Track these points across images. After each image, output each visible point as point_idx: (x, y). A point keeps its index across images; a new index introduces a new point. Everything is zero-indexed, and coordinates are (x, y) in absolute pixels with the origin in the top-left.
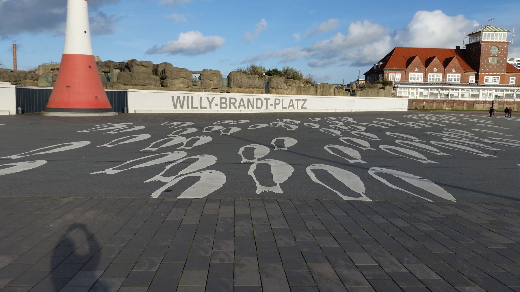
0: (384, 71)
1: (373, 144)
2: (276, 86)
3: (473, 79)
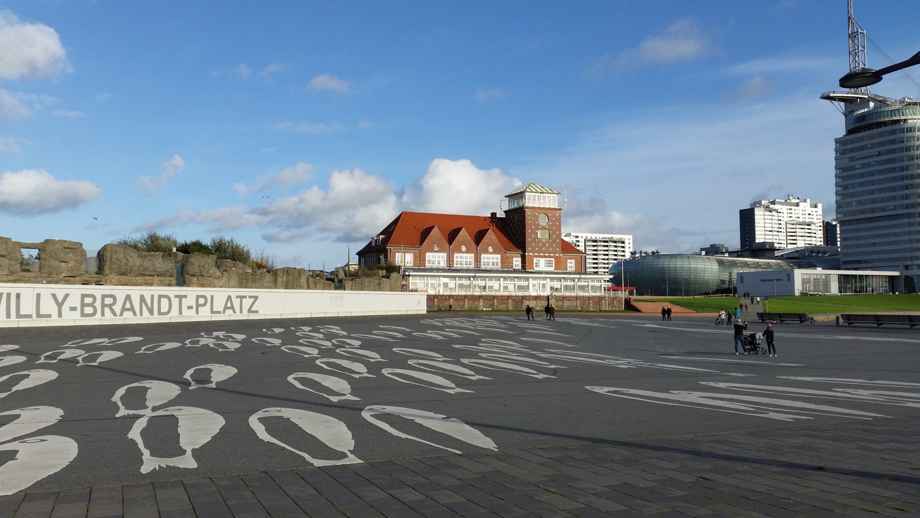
0: (387, 249)
1: (373, 367)
2: (198, 271)
3: (572, 265)
